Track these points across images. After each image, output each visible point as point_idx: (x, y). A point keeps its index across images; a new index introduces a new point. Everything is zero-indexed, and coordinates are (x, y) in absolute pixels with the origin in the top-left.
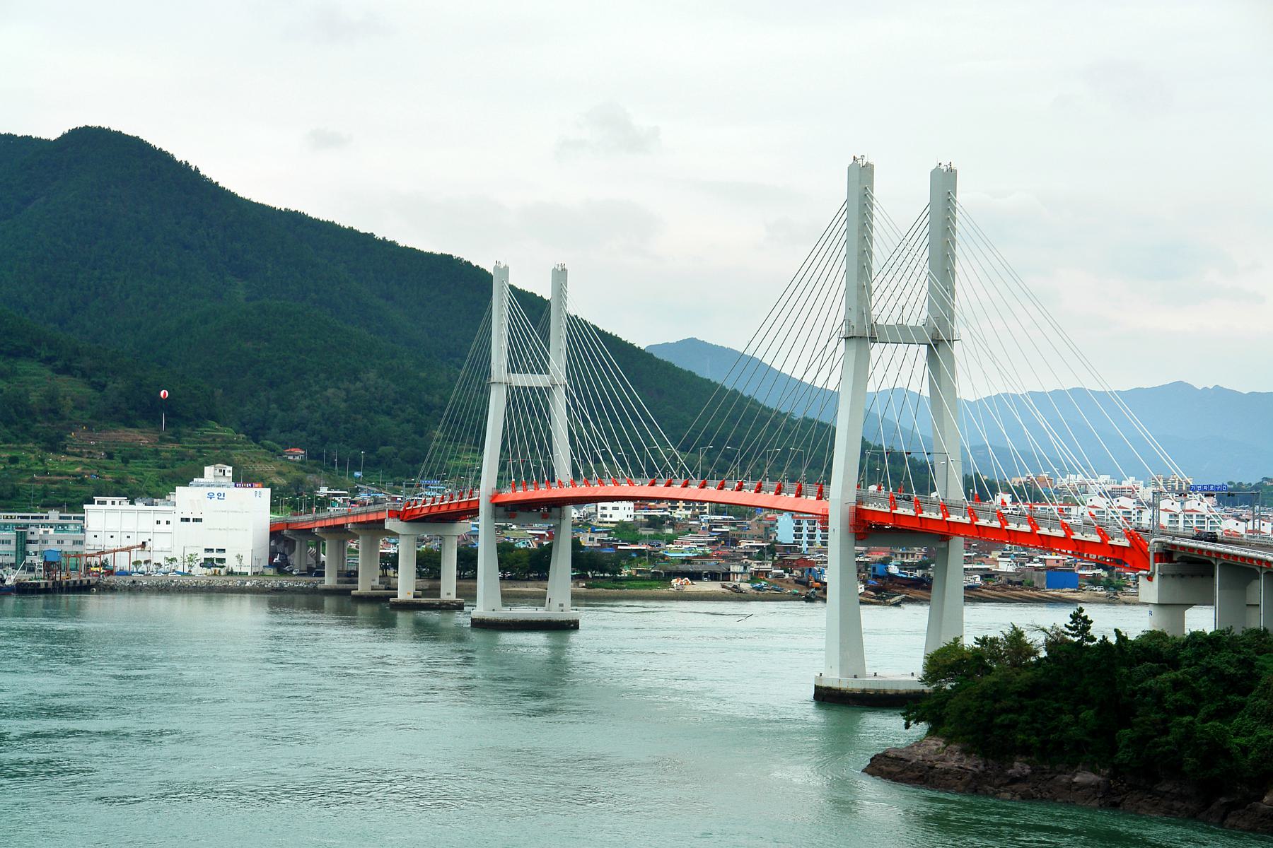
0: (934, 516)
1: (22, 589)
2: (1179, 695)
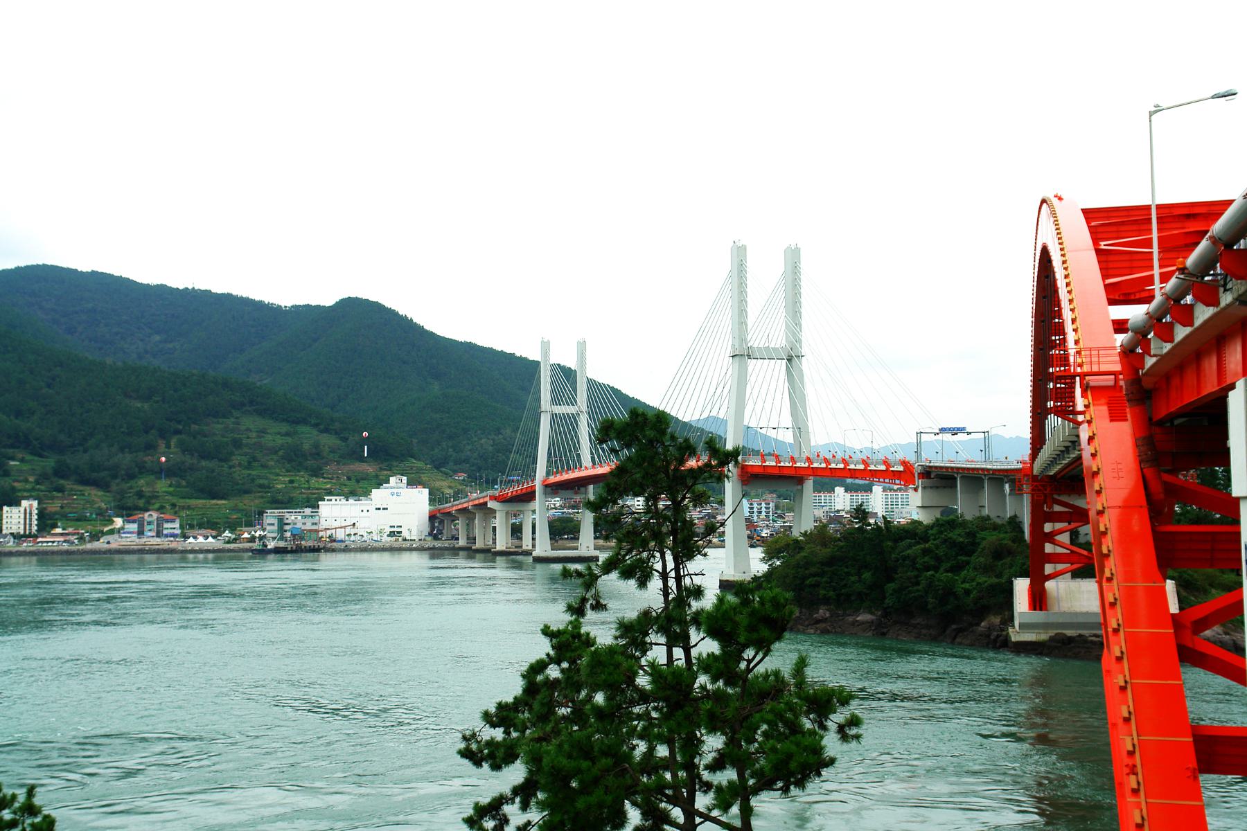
0: (787, 464)
1: (277, 551)
2: (926, 559)
